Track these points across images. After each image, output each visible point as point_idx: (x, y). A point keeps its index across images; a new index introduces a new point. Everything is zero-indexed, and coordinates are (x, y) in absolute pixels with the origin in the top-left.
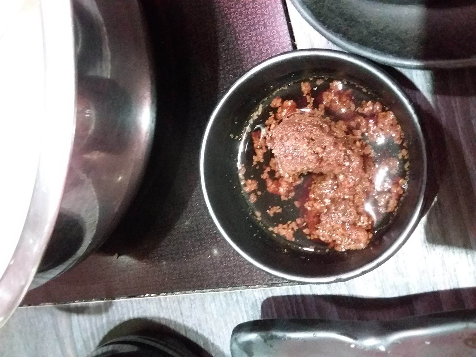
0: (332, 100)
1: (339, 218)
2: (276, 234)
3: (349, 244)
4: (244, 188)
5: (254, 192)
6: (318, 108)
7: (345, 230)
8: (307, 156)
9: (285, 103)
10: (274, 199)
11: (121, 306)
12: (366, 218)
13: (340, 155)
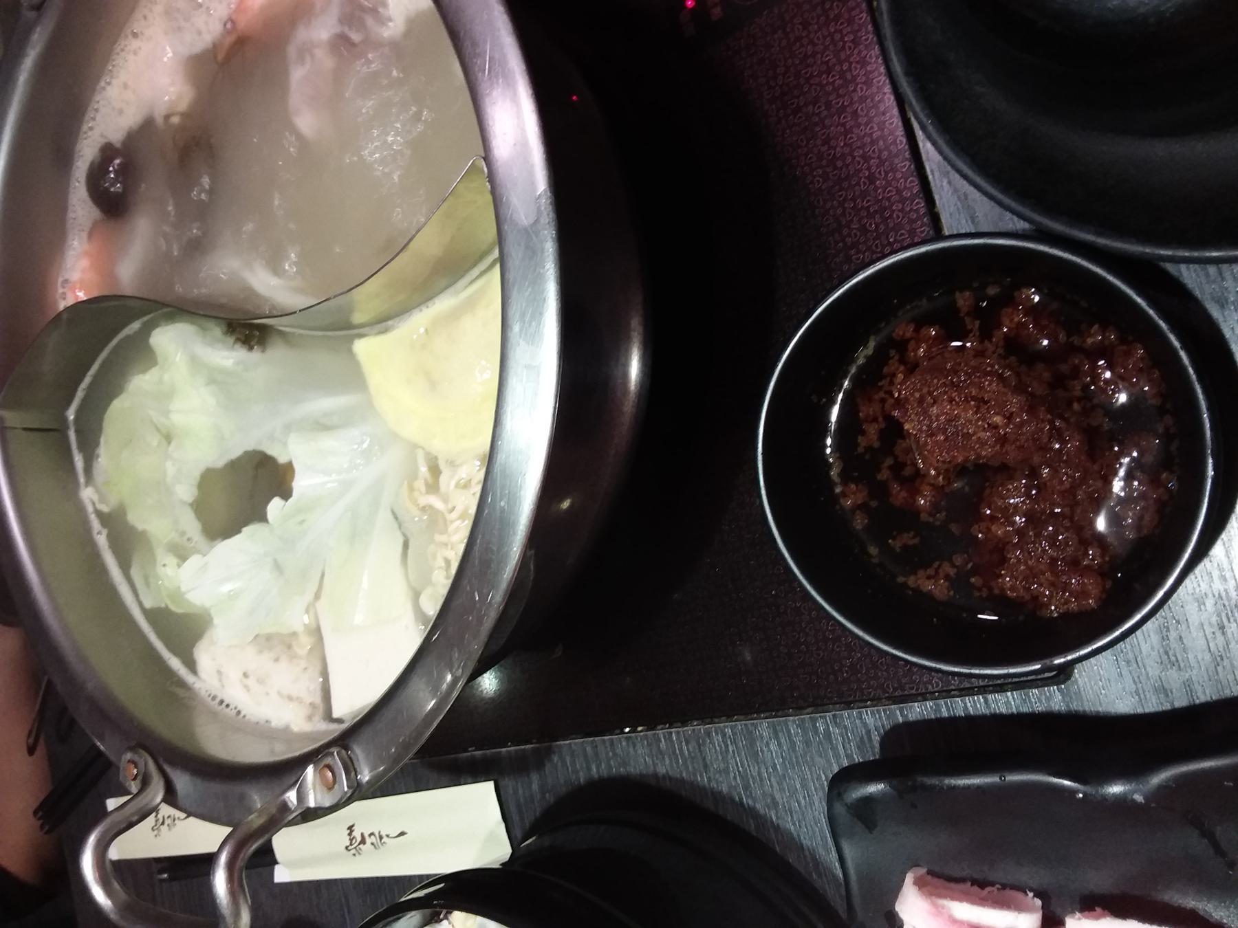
0: (1020, 324)
1: (1044, 551)
2: (912, 589)
3: (1066, 603)
4: (842, 501)
5: (862, 507)
6: (990, 338)
7: (1055, 573)
8: (975, 433)
9: (923, 331)
10: (908, 518)
11: (573, 756)
12: (1098, 551)
13: (1042, 430)
